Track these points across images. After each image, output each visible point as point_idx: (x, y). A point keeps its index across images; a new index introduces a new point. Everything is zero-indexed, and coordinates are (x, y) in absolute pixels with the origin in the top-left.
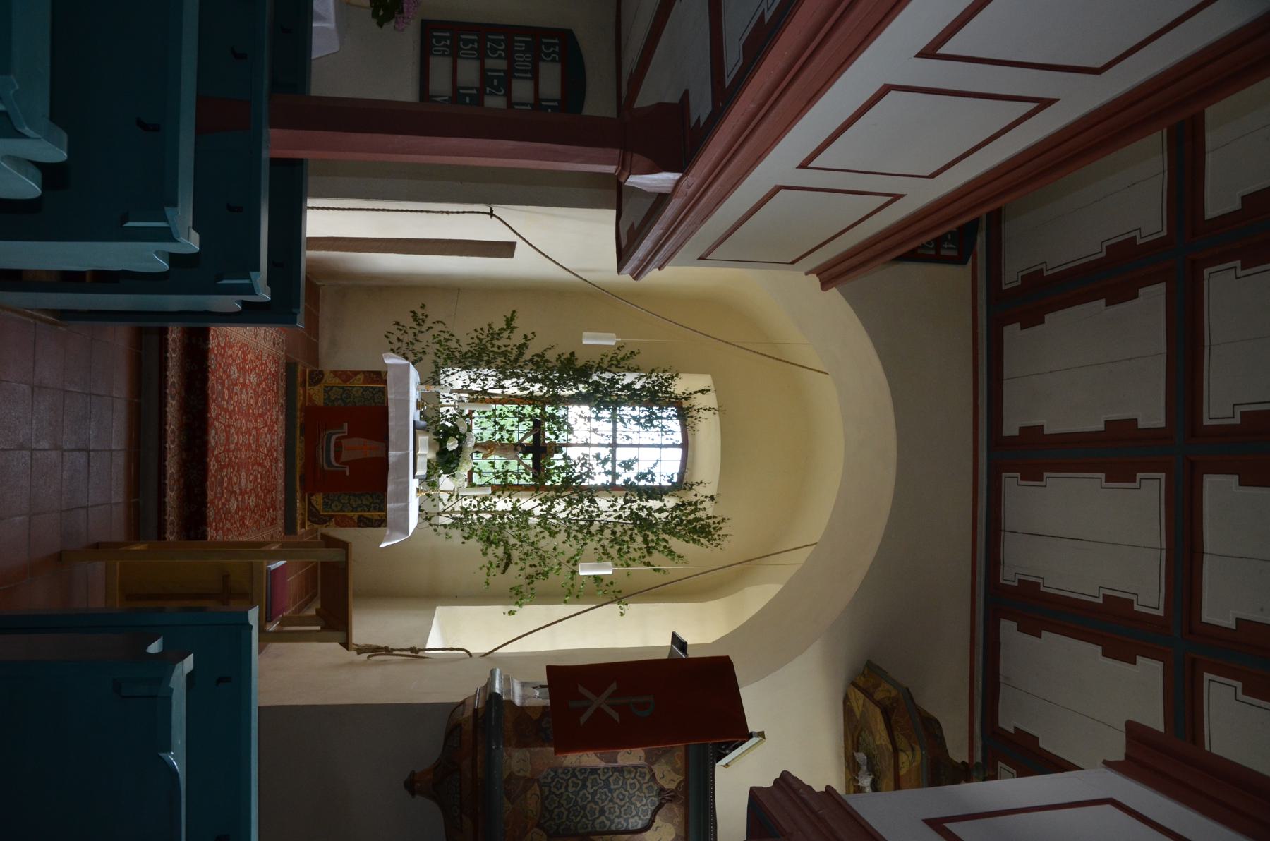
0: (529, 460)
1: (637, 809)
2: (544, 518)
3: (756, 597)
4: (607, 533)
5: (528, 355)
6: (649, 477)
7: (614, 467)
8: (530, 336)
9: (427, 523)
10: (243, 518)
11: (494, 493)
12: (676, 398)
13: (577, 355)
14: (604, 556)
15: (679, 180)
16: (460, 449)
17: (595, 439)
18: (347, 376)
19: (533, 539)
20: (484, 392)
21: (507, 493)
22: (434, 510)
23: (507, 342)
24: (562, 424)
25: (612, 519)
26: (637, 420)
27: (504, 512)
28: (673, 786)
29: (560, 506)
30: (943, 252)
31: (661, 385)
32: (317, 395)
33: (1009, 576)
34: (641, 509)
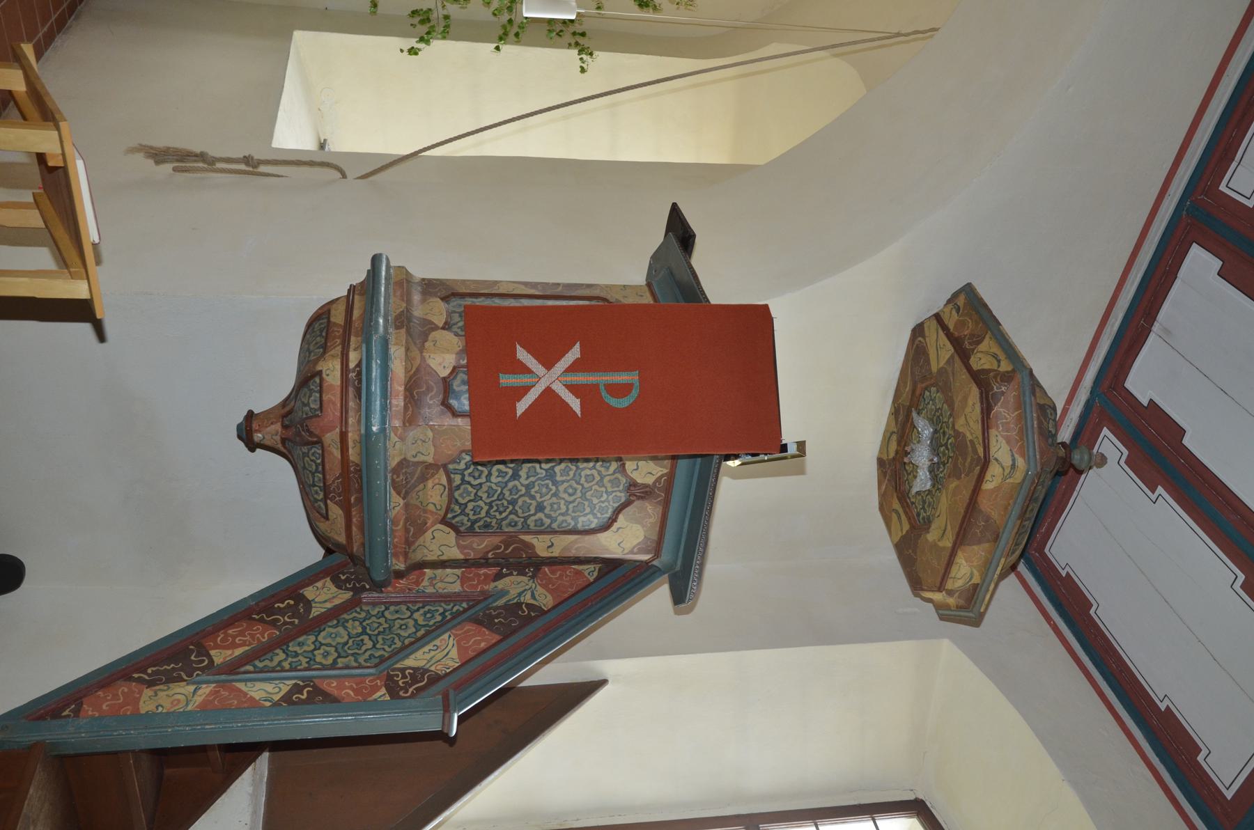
1: (593, 507)
28: (650, 480)
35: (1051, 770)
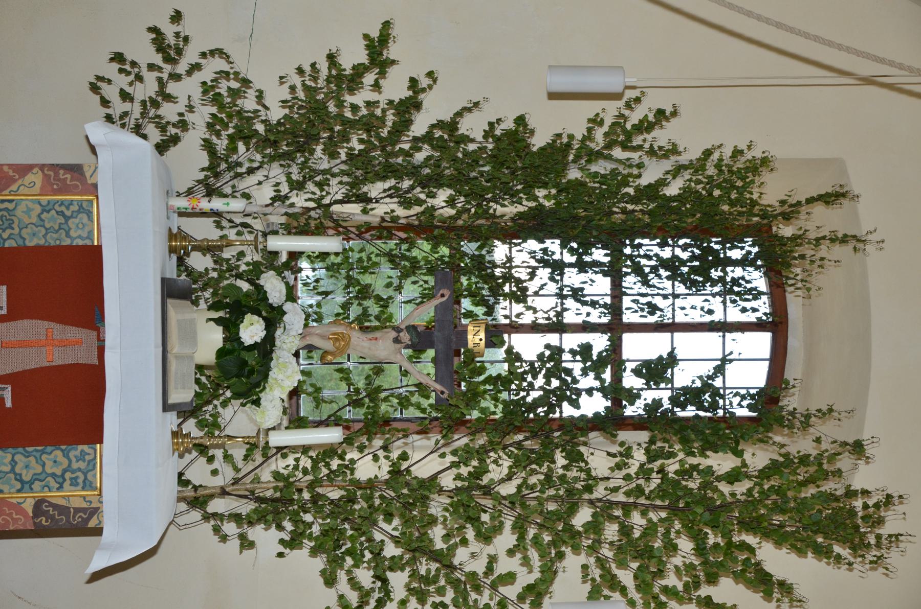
7: (617, 377)
8: (424, 82)
9: (196, 515)
12: (764, 215)
13: (532, 123)
17: (574, 314)
23: (373, 96)
24: (496, 284)
25: (620, 497)
27: (371, 484)
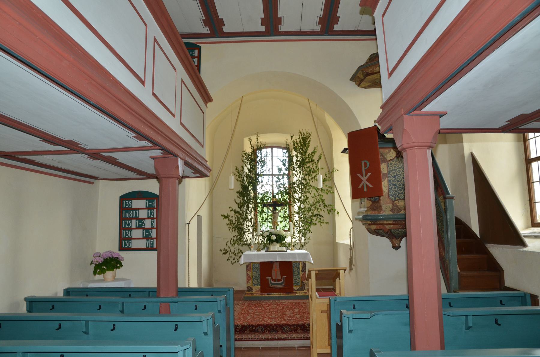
0: (279, 208)
2: (301, 202)
3: (330, 121)
4: (306, 177)
5: (238, 210)
6: (284, 161)
8: (231, 209)
9: (304, 247)
10: (303, 313)
11: (292, 221)
14: (315, 178)
15: (181, 159)
16: (276, 235)
17: (270, 183)
18: (249, 278)
19: (309, 206)
20: (253, 226)
21: (292, 216)
22: (299, 244)
23: (234, 218)
24: (265, 195)
25: (301, 175)
26: (262, 166)
29: (297, 196)
30: (197, 55)
31: (248, 157)
32: (257, 289)
33: (317, 28)
34: (297, 164)
35: (359, 120)
